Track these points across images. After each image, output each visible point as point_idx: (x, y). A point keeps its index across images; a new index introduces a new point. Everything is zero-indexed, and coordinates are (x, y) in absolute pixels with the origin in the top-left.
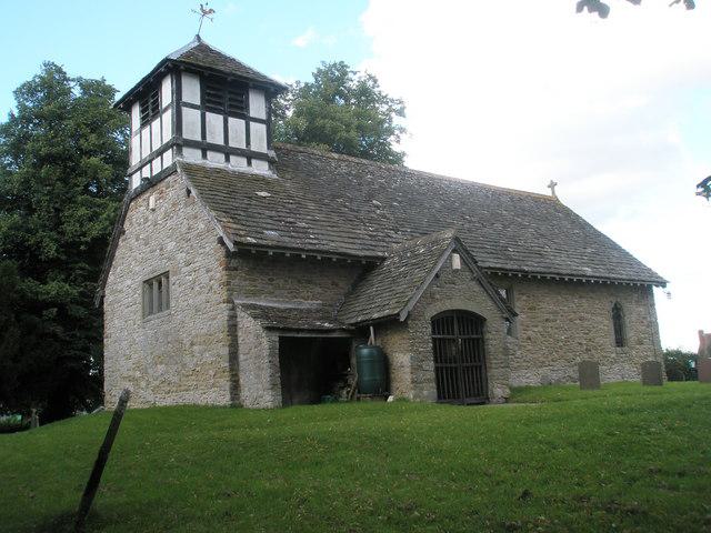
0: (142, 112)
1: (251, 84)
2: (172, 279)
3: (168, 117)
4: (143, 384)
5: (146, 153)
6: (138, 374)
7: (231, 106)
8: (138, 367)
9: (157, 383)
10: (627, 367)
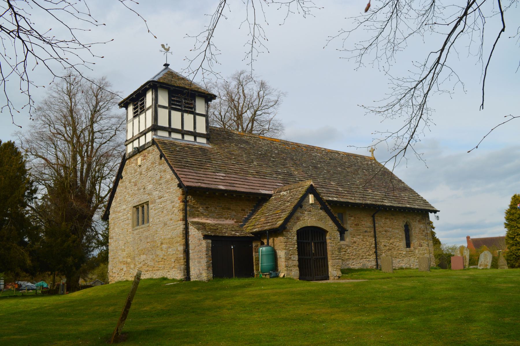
0: (134, 109)
1: (197, 94)
2: (151, 206)
3: (149, 113)
4: (132, 266)
5: (136, 133)
6: (129, 260)
7: (185, 107)
8: (129, 256)
9: (141, 265)
10: (413, 259)
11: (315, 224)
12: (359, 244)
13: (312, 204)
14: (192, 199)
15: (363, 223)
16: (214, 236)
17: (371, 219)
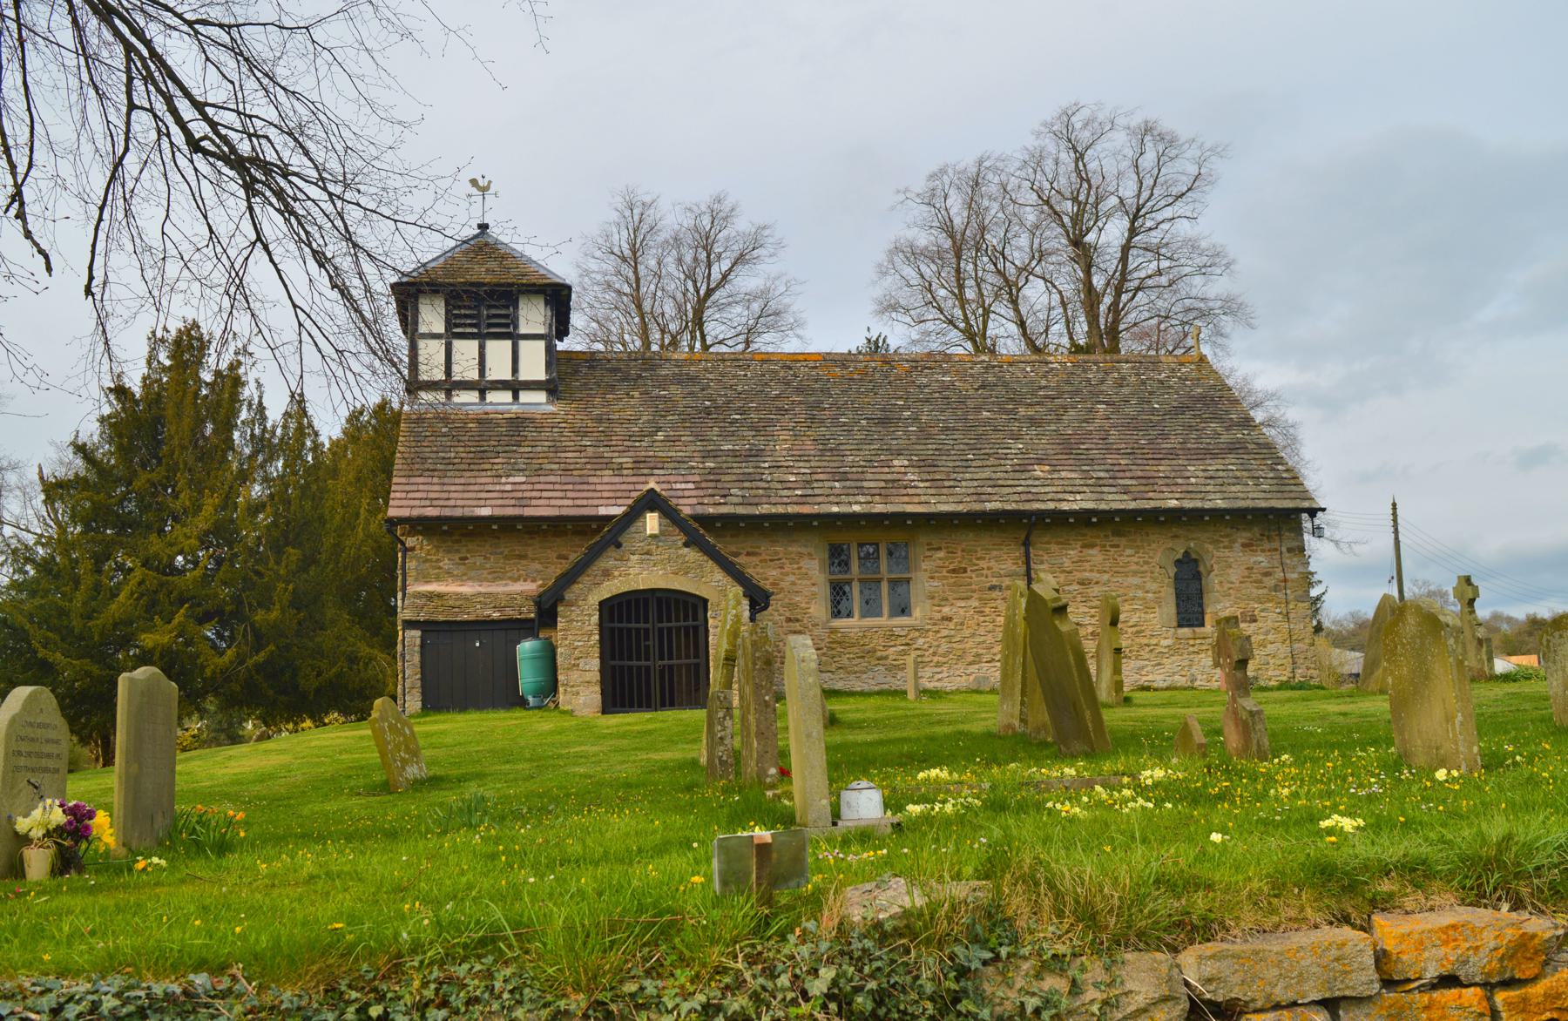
11: (662, 585)
12: (962, 624)
13: (653, 536)
14: (425, 543)
15: (983, 564)
16: (426, 622)
17: (1019, 552)
